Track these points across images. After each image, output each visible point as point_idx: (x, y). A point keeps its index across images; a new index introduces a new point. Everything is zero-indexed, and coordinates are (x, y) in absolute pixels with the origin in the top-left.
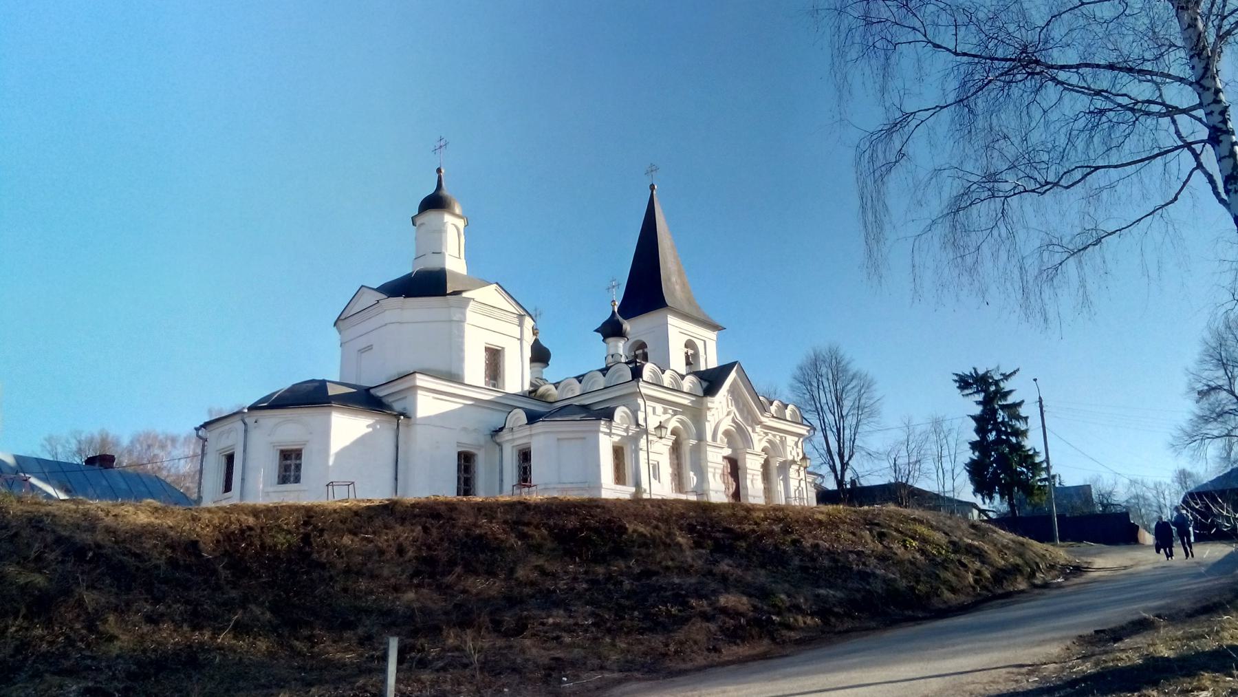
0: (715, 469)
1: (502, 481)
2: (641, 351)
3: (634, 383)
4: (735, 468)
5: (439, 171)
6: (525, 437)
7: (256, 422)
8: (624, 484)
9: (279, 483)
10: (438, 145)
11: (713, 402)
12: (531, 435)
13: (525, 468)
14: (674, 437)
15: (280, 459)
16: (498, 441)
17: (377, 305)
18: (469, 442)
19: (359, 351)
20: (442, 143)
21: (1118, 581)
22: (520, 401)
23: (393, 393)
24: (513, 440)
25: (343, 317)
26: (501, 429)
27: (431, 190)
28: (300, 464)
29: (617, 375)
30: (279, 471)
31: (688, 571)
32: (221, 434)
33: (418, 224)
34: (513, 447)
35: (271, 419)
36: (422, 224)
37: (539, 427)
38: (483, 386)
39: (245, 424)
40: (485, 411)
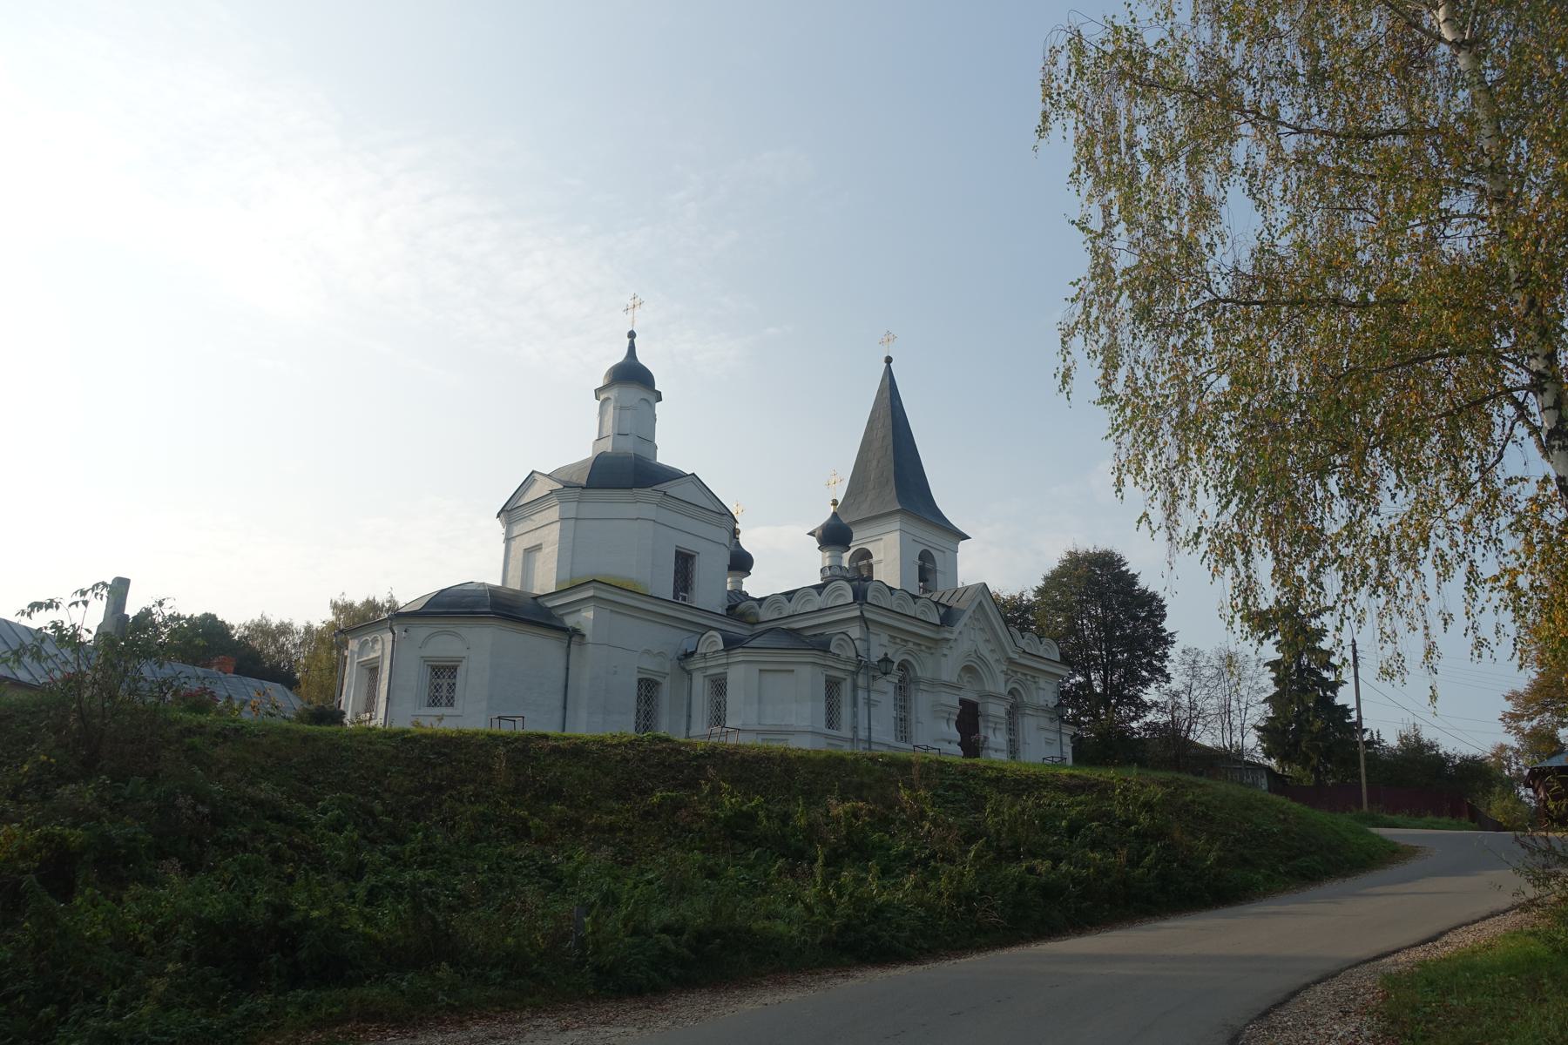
1: (690, 716)
5: (632, 335)
9: (429, 705)
11: (952, 633)
16: (688, 668)
18: (650, 664)
24: (706, 668)
26: (692, 654)
27: (620, 356)
34: (705, 676)
35: (421, 631)
37: (738, 655)
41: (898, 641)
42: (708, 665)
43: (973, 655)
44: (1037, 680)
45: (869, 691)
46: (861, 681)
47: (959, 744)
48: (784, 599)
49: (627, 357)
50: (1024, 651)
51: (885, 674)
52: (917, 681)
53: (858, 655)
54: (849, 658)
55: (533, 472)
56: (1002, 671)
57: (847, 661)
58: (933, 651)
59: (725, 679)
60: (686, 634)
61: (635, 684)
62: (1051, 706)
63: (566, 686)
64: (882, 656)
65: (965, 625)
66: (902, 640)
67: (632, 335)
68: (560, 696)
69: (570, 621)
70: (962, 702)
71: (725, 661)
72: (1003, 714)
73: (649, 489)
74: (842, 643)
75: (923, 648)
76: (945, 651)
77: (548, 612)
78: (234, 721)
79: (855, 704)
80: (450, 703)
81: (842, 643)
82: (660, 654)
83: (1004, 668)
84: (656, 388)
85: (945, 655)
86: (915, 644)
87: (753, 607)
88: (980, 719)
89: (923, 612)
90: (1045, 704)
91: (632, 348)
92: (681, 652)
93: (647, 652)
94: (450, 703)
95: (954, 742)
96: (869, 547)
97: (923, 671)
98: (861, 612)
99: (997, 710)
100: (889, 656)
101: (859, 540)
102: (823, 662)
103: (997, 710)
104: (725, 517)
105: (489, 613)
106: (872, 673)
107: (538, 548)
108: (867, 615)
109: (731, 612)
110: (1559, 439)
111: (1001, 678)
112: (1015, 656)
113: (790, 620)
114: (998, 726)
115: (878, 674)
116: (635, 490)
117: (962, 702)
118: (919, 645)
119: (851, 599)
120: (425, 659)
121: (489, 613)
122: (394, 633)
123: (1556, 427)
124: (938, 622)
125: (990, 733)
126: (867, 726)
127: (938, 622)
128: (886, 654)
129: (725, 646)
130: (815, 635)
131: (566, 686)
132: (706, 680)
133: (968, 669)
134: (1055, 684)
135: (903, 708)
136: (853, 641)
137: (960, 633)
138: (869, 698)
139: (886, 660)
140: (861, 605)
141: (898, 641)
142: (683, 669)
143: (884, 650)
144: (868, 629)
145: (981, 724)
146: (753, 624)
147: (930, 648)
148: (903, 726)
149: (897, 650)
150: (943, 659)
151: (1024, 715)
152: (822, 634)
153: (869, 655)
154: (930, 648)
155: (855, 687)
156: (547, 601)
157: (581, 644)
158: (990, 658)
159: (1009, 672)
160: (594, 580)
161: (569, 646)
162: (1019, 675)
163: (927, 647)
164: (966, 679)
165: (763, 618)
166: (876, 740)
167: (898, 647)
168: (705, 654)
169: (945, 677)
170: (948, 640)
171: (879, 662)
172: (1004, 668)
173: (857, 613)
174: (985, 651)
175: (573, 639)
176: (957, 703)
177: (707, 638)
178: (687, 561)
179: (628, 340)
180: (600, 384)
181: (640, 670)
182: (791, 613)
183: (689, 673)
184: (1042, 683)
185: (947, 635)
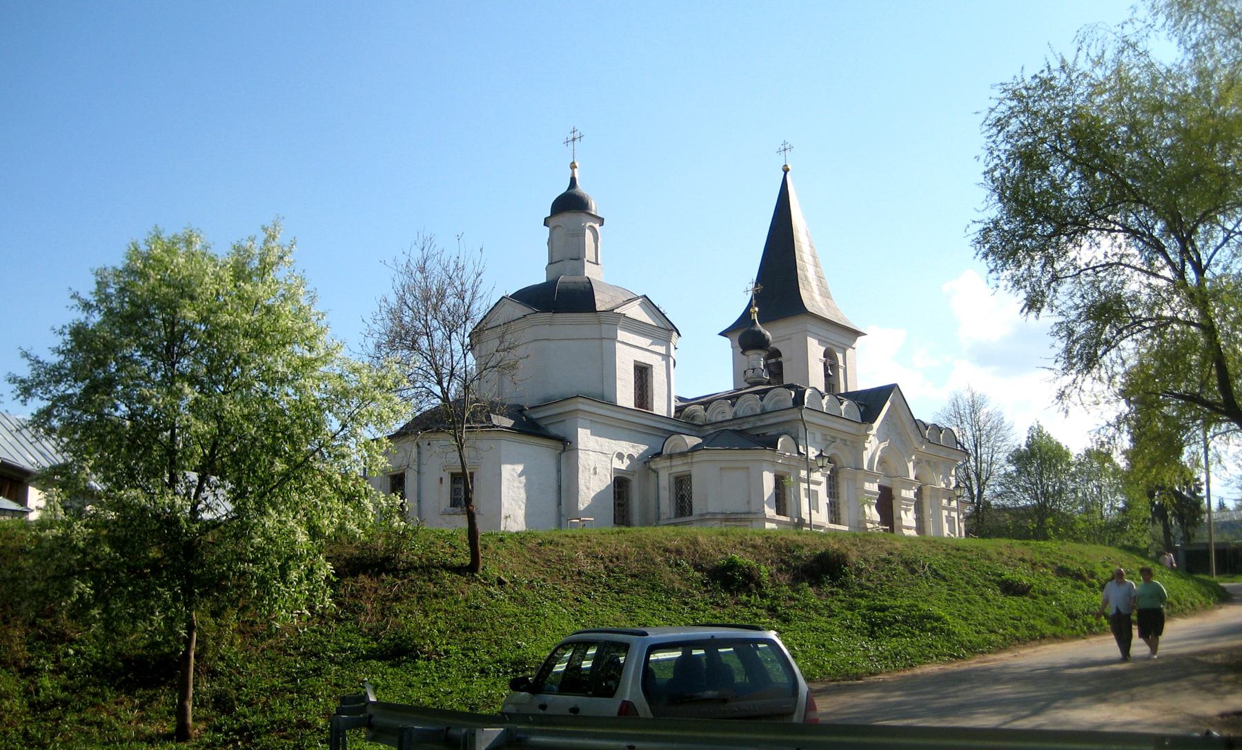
3: (796, 410)
4: (886, 503)
7: (429, 444)
8: (628, 524)
9: (676, 517)
10: (571, 137)
13: (682, 497)
17: (523, 320)
20: (577, 135)
21: (995, 712)
22: (668, 424)
23: (561, 414)
27: (563, 188)
29: (775, 399)
34: (670, 474)
38: (633, 407)
40: (651, 437)
70: (880, 487)
91: (573, 181)
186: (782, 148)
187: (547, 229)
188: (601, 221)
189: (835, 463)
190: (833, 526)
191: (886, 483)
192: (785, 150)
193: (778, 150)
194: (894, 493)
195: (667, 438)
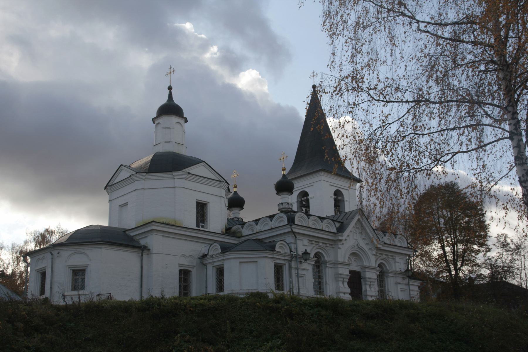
0: (344, 279)
1: (207, 288)
2: (305, 198)
5: (170, 88)
6: (220, 261)
7: (58, 253)
9: (72, 290)
11: (342, 236)
12: (224, 260)
14: (316, 259)
15: (73, 276)
16: (204, 263)
18: (185, 262)
19: (120, 206)
24: (213, 262)
25: (110, 184)
26: (206, 255)
27: (164, 100)
28: (84, 278)
30: (72, 283)
31: (499, 100)
32: (39, 259)
33: (156, 122)
34: (213, 267)
35: (66, 253)
36: (159, 123)
37: (230, 255)
39: (52, 254)
41: (313, 242)
42: (214, 260)
43: (357, 247)
44: (394, 258)
45: (298, 270)
46: (293, 264)
47: (350, 294)
48: (253, 223)
49: (168, 100)
50: (385, 243)
51: (306, 260)
52: (325, 262)
53: (291, 251)
54: (285, 253)
55: (121, 165)
56: (373, 255)
57: (285, 255)
58: (334, 246)
59: (223, 268)
60: (203, 245)
61: (178, 272)
62: (403, 271)
63: (142, 276)
64: (304, 251)
65: (351, 231)
66: (316, 242)
67: (170, 88)
68: (138, 281)
69: (143, 242)
70: (351, 272)
71: (222, 258)
72: (375, 277)
73: (180, 172)
74: (282, 246)
75: (328, 245)
76: (340, 246)
77: (131, 239)
78: (441, 27)
79: (290, 276)
80: (83, 288)
81: (282, 246)
82: (190, 256)
83: (374, 253)
84: (185, 116)
85: (340, 248)
86: (323, 243)
87: (239, 229)
88: (362, 280)
89: (327, 226)
90: (399, 270)
91: (170, 96)
92: (201, 254)
93: (183, 256)
94: (83, 288)
95: (347, 293)
96: (306, 190)
97: (328, 257)
98: (292, 229)
99: (371, 275)
100: (307, 251)
101: (299, 186)
102: (272, 256)
103: (371, 275)
104: (222, 183)
105: (100, 241)
106: (299, 260)
107: (126, 204)
108: (294, 230)
109: (228, 232)
110: (519, 161)
111: (373, 258)
112: (379, 246)
113: (257, 235)
114: (372, 283)
115: (303, 260)
116: (173, 173)
117: (351, 272)
118: (326, 244)
119: (286, 223)
120: (69, 267)
121: (100, 241)
122: (52, 254)
123: (517, 155)
124: (335, 231)
125: (368, 288)
126: (297, 287)
127: (335, 231)
128: (306, 250)
129: (222, 251)
130: (270, 242)
131: (142, 276)
132: (214, 268)
133: (353, 254)
134: (405, 259)
135: (319, 277)
136: (288, 244)
137: (348, 236)
138: (298, 273)
139: (306, 253)
140: (291, 225)
141: (313, 242)
142: (202, 263)
143: (305, 248)
144: (296, 237)
145: (363, 283)
146: (239, 237)
147: (332, 245)
148: (319, 285)
149: (314, 247)
150: (339, 250)
151: (388, 276)
152: (274, 241)
153: (297, 251)
154: (332, 245)
155: (290, 268)
156: (131, 232)
157: (148, 254)
158: (366, 248)
159: (378, 254)
160: (153, 221)
161: (142, 256)
162: (384, 256)
163: (330, 244)
164: (353, 260)
165: (244, 234)
166: (302, 295)
167: (314, 245)
168: (212, 255)
169: (340, 259)
170: (341, 240)
171: (302, 254)
172: (374, 253)
173: (289, 230)
174: (362, 244)
175: (144, 252)
176: (347, 273)
177: (214, 246)
178: (203, 208)
179: (168, 91)
180: (155, 116)
181: (180, 265)
182: (258, 231)
183: (205, 265)
184: (397, 259)
185: (340, 238)
186: (312, 75)
187: (154, 125)
188: (186, 121)
189: (382, 268)
190: (278, 292)
191: (355, 268)
192: (314, 76)
193: (310, 76)
194: (362, 275)
195: (211, 245)
